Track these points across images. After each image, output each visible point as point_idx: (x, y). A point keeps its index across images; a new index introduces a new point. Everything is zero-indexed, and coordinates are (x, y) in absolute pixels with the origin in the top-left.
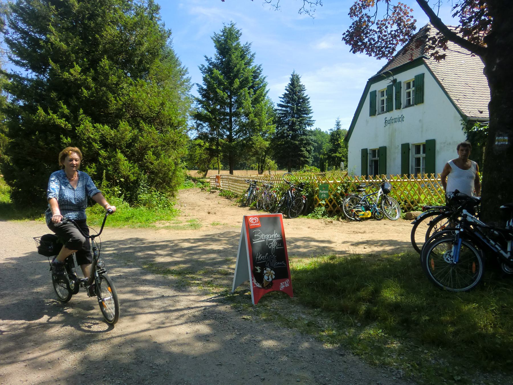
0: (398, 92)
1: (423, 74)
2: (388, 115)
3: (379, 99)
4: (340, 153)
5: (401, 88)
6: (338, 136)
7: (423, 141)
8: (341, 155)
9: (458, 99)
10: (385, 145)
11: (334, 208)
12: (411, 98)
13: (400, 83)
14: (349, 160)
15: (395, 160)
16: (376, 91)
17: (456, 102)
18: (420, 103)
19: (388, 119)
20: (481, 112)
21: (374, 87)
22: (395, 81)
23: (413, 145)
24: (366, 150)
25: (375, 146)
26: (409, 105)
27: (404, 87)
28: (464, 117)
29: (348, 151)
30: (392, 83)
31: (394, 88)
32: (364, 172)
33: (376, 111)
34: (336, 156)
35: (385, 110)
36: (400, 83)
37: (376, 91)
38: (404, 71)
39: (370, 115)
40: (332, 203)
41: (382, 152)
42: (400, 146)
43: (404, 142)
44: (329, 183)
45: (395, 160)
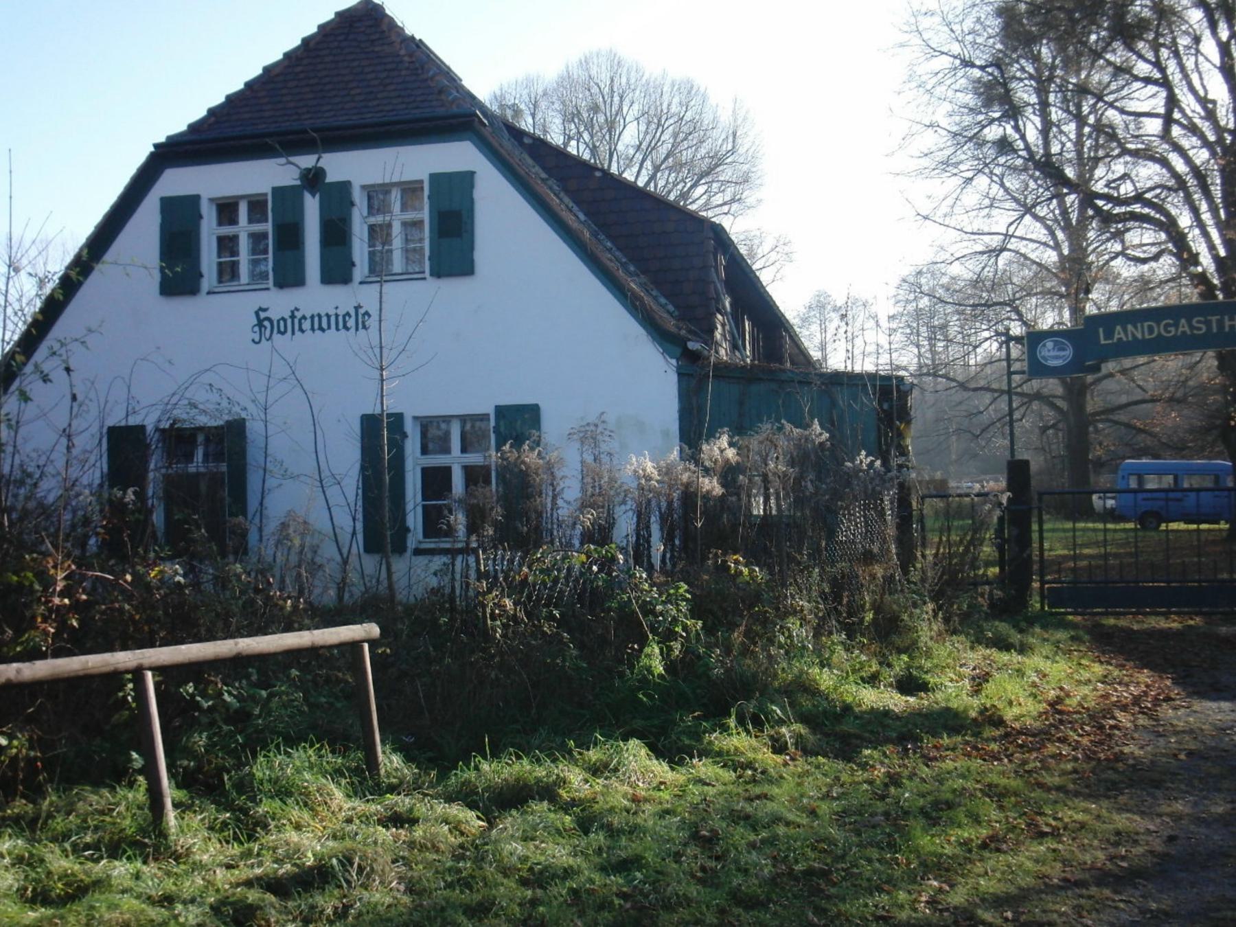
1: (472, 174)
2: (279, 303)
3: (209, 229)
22: (313, 179)
30: (298, 183)
36: (345, 186)
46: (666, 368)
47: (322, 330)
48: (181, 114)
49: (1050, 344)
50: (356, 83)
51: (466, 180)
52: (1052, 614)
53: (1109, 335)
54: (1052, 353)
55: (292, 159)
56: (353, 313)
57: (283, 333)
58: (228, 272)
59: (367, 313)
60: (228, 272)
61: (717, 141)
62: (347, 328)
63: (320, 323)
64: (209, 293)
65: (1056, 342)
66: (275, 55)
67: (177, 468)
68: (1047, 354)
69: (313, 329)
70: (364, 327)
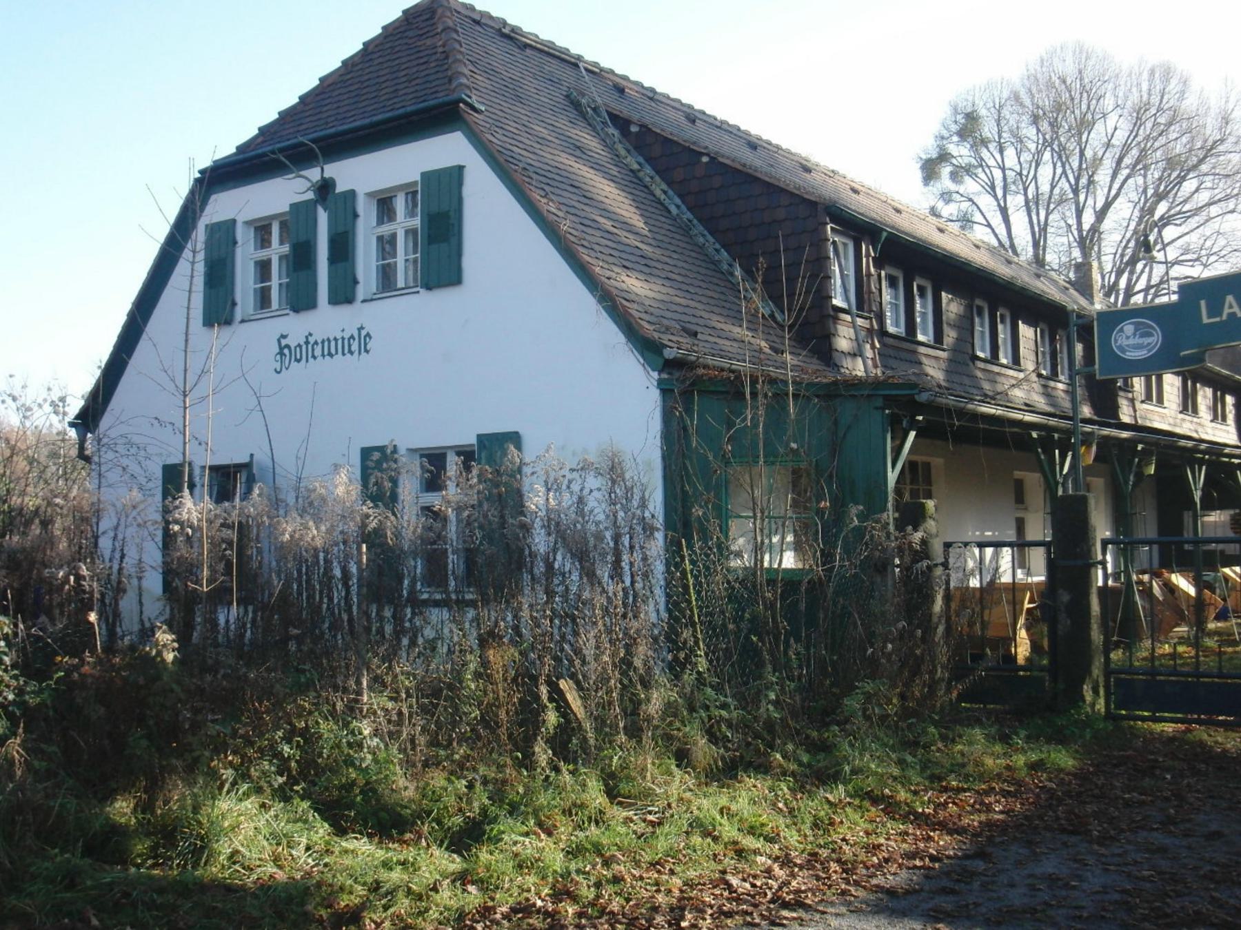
1: (461, 169)
2: (297, 327)
3: (246, 255)
13: (351, 194)
16: (234, 221)
22: (325, 188)
27: (366, 213)
30: (310, 195)
36: (351, 194)
39: (209, 322)
46: (648, 384)
47: (330, 355)
48: (227, 137)
49: (1129, 328)
50: (405, 84)
51: (455, 175)
53: (1215, 310)
54: (1131, 341)
55: (303, 173)
56: (356, 336)
57: (299, 361)
59: (368, 335)
60: (263, 299)
61: (1211, 131)
62: (351, 352)
64: (243, 321)
65: (1137, 326)
66: (333, 64)
68: (1126, 342)
69: (323, 355)
70: (367, 351)
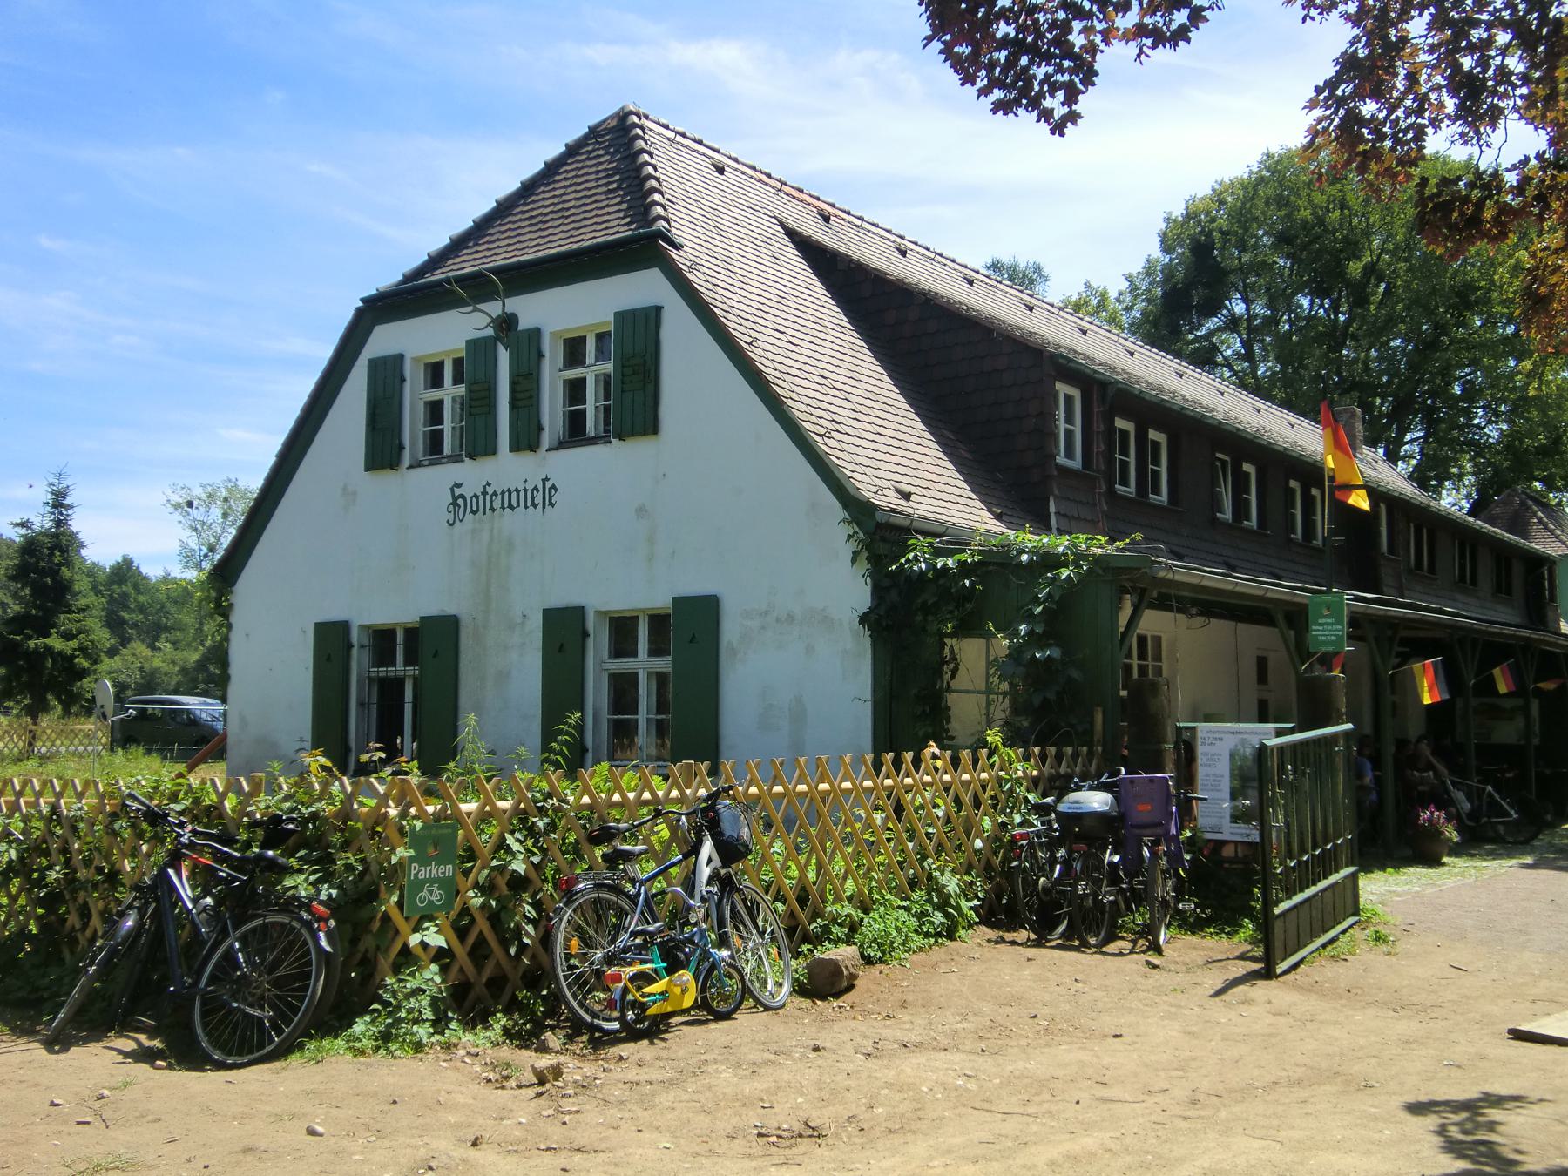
0: (528, 376)
2: (471, 475)
3: (415, 395)
4: (68, 636)
5: (541, 355)
6: (58, 558)
7: (661, 601)
8: (74, 644)
9: (823, 431)
10: (450, 610)
11: (479, 967)
12: (447, 427)
13: (535, 334)
14: (234, 671)
15: (504, 685)
17: (824, 446)
18: (645, 433)
19: (467, 491)
20: (907, 496)
21: (385, 339)
22: (507, 324)
23: (601, 614)
24: (344, 626)
25: (398, 608)
26: (575, 433)
28: (858, 509)
29: (230, 627)
30: (490, 331)
31: (504, 356)
32: (330, 732)
33: (401, 448)
34: (48, 649)
35: (447, 450)
36: (535, 334)
37: (402, 356)
38: (404, 318)
40: (471, 940)
41: (433, 643)
42: (537, 621)
43: (559, 599)
44: (458, 818)
45: (504, 685)
47: (511, 507)
52: (1132, 781)
55: (480, 306)
58: (622, 733)
59: (553, 487)
62: (535, 506)
63: (511, 500)
67: (383, 671)
69: (503, 508)
70: (552, 505)
